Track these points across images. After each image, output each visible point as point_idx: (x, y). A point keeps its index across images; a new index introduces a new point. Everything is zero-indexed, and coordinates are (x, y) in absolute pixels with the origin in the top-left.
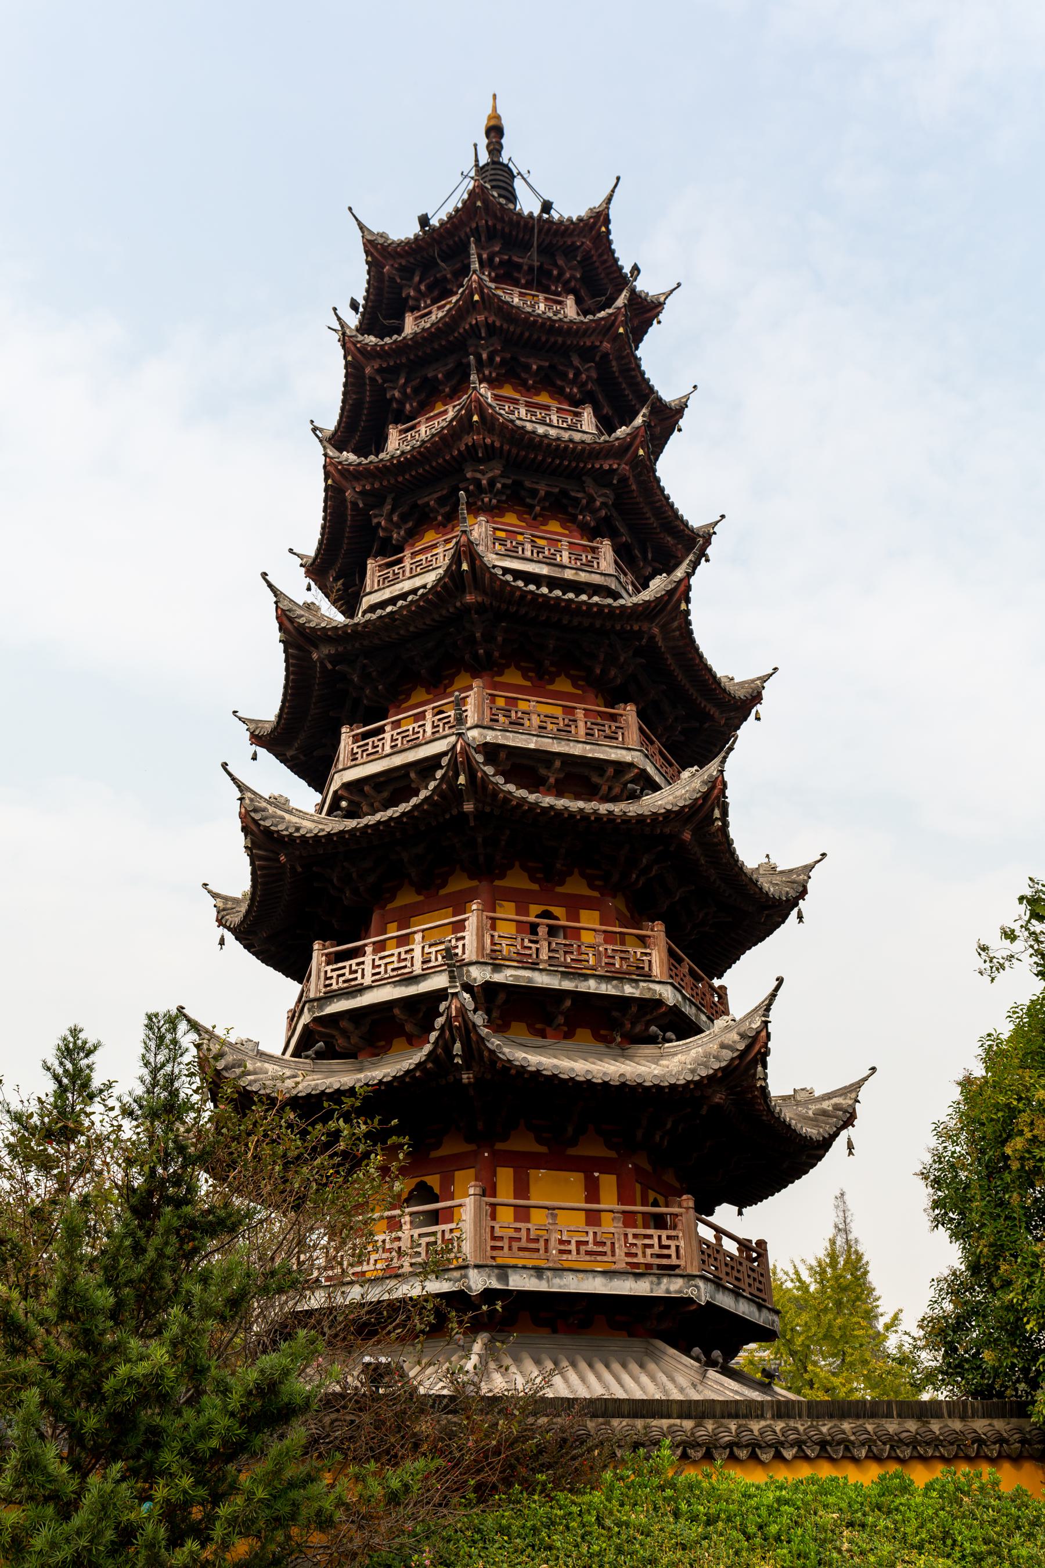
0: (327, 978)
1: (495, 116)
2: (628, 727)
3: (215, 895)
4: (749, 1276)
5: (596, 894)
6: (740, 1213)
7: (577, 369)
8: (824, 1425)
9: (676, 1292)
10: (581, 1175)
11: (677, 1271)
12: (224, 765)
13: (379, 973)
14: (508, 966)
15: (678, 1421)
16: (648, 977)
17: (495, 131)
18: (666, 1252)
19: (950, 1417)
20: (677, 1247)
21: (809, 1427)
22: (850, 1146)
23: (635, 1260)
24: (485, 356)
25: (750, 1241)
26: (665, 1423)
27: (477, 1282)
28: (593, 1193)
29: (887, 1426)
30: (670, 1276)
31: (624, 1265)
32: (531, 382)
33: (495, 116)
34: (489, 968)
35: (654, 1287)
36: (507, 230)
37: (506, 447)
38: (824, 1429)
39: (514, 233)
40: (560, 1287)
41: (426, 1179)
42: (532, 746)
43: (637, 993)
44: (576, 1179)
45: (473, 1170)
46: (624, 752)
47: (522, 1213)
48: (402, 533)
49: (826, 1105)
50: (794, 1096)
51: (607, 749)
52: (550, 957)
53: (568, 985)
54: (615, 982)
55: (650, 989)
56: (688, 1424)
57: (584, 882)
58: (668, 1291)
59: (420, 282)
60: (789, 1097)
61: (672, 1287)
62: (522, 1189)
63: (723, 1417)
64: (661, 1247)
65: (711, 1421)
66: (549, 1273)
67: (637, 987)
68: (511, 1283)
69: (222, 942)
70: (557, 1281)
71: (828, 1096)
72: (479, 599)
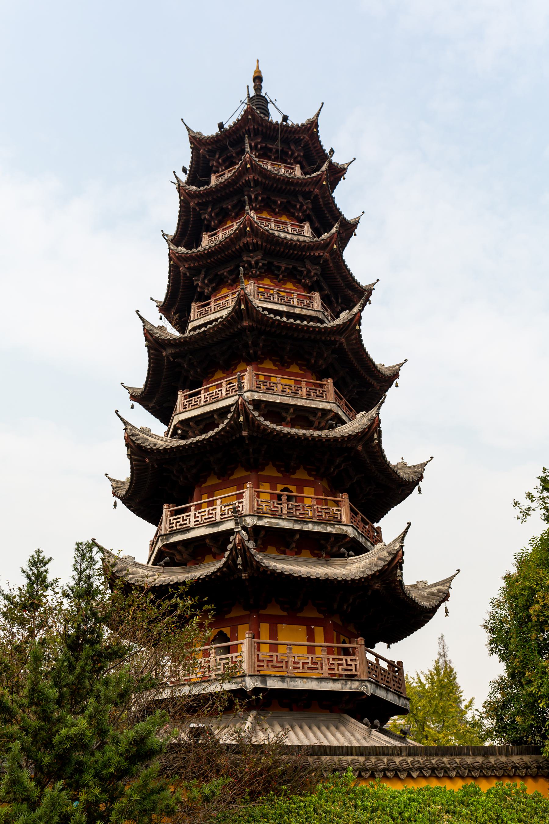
0: (171, 524)
1: (258, 71)
2: (329, 391)
3: (111, 480)
4: (393, 680)
5: (312, 479)
6: (389, 647)
7: (301, 203)
8: (434, 759)
9: (355, 689)
10: (305, 627)
11: (356, 678)
12: (117, 412)
13: (198, 521)
14: (266, 517)
15: (356, 758)
16: (339, 522)
17: (258, 79)
18: (349, 668)
19: (500, 754)
20: (356, 665)
21: (426, 760)
22: (447, 612)
23: (333, 672)
24: (253, 196)
25: (394, 662)
26: (349, 758)
27: (250, 684)
28: (311, 637)
29: (467, 759)
30: (352, 680)
31: (328, 675)
32: (277, 210)
33: (258, 71)
34: (256, 518)
35: (344, 686)
36: (264, 131)
37: (264, 244)
38: (434, 761)
39: (268, 132)
40: (294, 686)
41: (223, 629)
42: (278, 401)
43: (334, 531)
44: (302, 629)
45: (248, 625)
46: (326, 404)
47: (274, 648)
48: (210, 289)
49: (434, 590)
50: (416, 585)
51: (318, 402)
52: (288, 512)
53: (297, 527)
54: (322, 525)
55: (341, 529)
56: (362, 759)
57: (306, 472)
58: (351, 688)
59: (219, 158)
60: (414, 586)
61: (353, 686)
62: (273, 635)
63: (380, 755)
64: (347, 665)
65: (374, 757)
66: (288, 679)
67: (334, 528)
68: (268, 684)
69: (115, 505)
70: (292, 683)
71: (435, 585)
72: (250, 324)
